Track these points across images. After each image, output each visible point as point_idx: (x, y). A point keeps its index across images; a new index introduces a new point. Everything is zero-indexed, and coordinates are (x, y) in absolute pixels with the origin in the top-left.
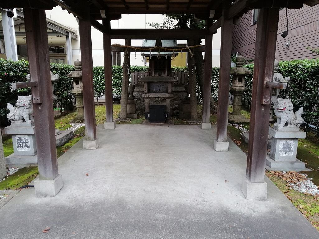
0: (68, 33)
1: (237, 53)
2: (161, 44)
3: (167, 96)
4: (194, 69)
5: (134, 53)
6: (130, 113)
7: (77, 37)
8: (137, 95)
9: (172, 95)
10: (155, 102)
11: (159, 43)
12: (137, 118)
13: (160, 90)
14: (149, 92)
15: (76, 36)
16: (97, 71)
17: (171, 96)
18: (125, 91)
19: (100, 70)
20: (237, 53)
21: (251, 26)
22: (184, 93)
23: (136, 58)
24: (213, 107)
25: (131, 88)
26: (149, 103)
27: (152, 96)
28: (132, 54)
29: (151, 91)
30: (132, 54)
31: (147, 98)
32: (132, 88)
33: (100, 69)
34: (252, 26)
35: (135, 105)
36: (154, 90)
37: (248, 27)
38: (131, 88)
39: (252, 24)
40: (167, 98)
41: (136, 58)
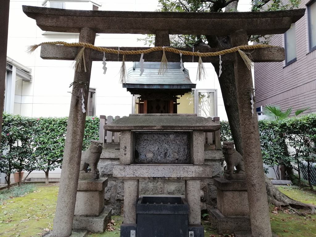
0: (11, 67)
1: (261, 107)
2: (167, 42)
3: (190, 171)
4: (253, 95)
5: (100, 63)
6: (87, 216)
7: (30, 79)
8: (109, 167)
9: (208, 169)
10: (149, 183)
11: (162, 40)
12: (102, 231)
13: (166, 153)
14: (136, 159)
15: (30, 76)
16: (48, 124)
17: (204, 171)
18: (71, 159)
19: (53, 123)
20: (261, 107)
21: (284, 68)
22: (214, 163)
23: (105, 73)
24: (272, 193)
25: (92, 150)
26: (134, 194)
27: (144, 171)
28: (96, 66)
29: (142, 157)
30: (96, 66)
31: (130, 179)
32: (94, 151)
33: (54, 121)
34: (285, 68)
35: (102, 192)
36: (150, 156)
37: (278, 70)
38: (92, 150)
39: (308, 51)
40: (193, 179)
41: (105, 73)
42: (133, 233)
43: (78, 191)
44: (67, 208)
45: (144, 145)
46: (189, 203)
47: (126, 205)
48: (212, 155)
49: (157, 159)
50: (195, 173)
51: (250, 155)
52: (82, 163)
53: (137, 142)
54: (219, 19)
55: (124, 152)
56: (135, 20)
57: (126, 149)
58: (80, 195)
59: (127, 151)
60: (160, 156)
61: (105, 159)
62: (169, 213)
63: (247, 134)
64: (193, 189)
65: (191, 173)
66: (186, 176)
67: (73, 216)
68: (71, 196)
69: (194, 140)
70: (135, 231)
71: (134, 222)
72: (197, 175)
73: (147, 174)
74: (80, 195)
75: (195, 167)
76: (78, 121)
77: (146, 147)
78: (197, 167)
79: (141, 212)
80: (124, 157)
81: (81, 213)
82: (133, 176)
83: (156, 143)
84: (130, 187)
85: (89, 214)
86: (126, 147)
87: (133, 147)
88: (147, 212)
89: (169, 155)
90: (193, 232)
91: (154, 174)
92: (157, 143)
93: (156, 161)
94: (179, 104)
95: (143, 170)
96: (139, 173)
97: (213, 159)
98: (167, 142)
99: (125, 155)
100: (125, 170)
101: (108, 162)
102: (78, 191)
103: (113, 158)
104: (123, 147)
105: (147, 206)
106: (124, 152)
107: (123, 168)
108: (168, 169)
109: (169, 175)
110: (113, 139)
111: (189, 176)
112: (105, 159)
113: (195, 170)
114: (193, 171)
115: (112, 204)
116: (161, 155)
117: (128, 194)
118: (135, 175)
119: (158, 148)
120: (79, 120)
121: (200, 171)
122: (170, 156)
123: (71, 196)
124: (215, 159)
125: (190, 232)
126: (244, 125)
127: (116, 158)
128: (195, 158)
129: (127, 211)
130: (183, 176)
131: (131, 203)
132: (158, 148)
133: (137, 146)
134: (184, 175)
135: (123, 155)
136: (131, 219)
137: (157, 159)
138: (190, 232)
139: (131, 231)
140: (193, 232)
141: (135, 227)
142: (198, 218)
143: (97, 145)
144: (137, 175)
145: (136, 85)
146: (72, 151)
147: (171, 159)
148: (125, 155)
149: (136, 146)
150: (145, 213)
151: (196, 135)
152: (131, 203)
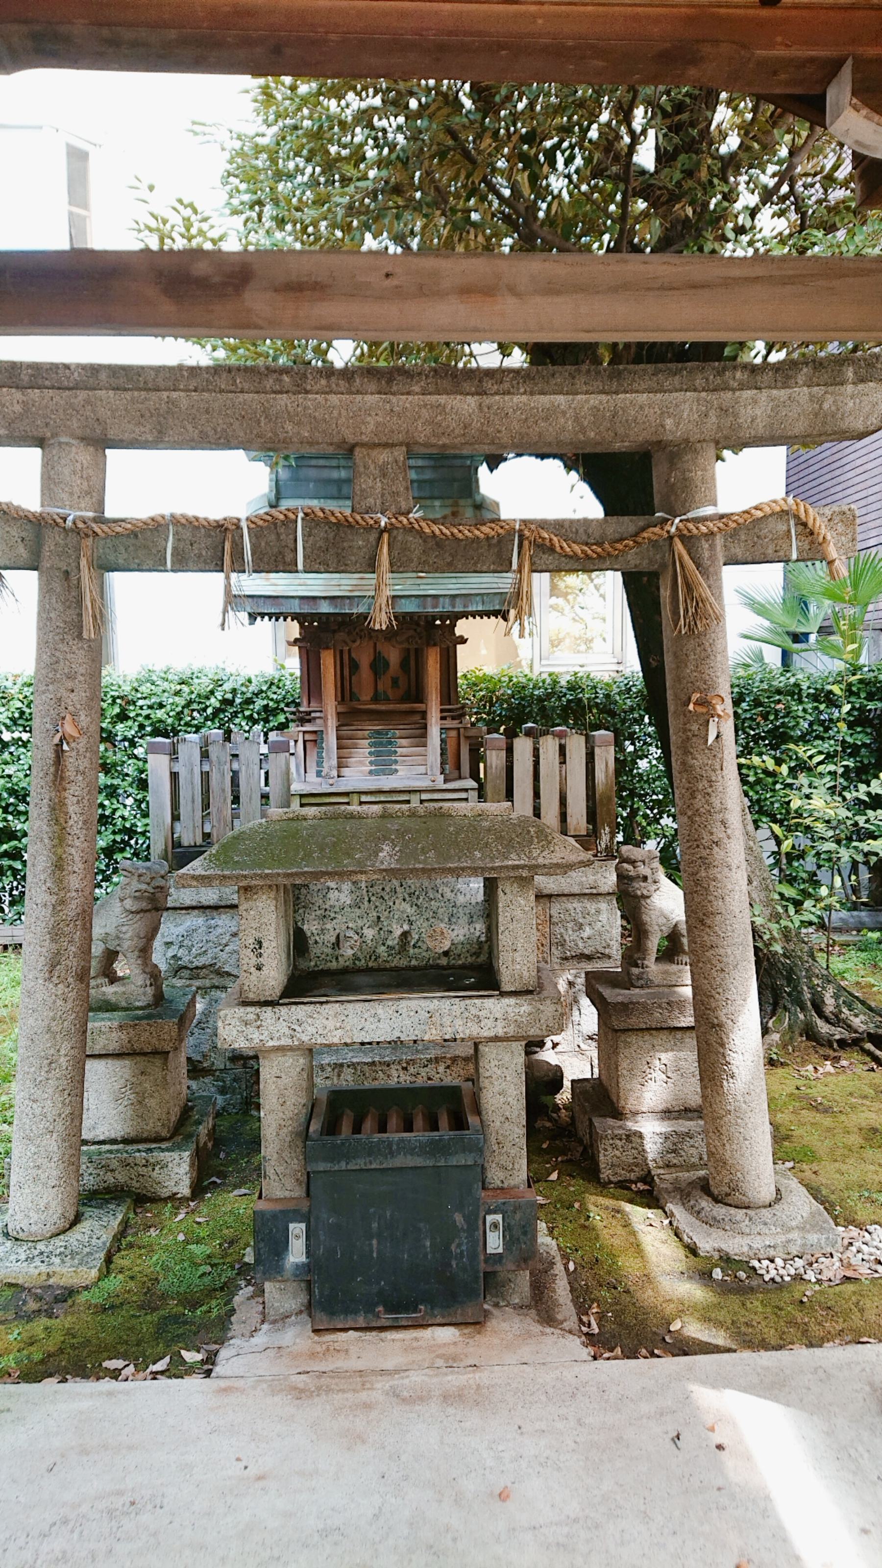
6: (126, 1141)
12: (184, 1190)
25: (129, 904)
42: (297, 1231)
43: (88, 1056)
44: (55, 1135)
45: (327, 907)
46: (485, 1118)
47: (268, 1136)
48: (584, 879)
49: (373, 958)
50: (503, 1024)
51: (708, 922)
52: (97, 949)
53: (298, 898)
54: (604, 397)
55: (254, 961)
56: (268, 401)
57: (260, 948)
58: (93, 1067)
59: (265, 955)
60: (384, 944)
61: (182, 909)
62: (419, 1161)
63: (698, 846)
64: (499, 1072)
65: (490, 1023)
66: (475, 1034)
67: (75, 1141)
68: (66, 1092)
69: (500, 910)
70: (303, 1226)
71: (299, 1192)
72: (511, 1030)
73: (339, 1033)
74: (93, 1067)
75: (506, 1001)
76: (71, 822)
77: (333, 915)
78: (512, 1001)
79: (322, 1166)
80: (253, 978)
81: (102, 1132)
82: (289, 1042)
83: (369, 901)
84: (283, 1075)
85: (133, 1134)
86: (260, 943)
87: (286, 916)
88: (343, 1165)
89: (418, 941)
90: (499, 1218)
91: (363, 1033)
92: (373, 899)
93: (370, 964)
94: (463, 641)
95: (324, 1021)
96: (311, 1030)
97: (587, 891)
98: (410, 895)
99: (259, 968)
100: (259, 1023)
101: (196, 921)
102: (88, 1056)
103: (211, 903)
104: (251, 941)
105: (343, 1144)
106: (254, 961)
107: (252, 1017)
108: (412, 1014)
109: (416, 1032)
110: (207, 829)
111: (485, 1034)
112: (182, 909)
113: (503, 1011)
114: (498, 1015)
115: (217, 1073)
116: (389, 943)
117: (275, 1100)
118: (299, 1039)
119: (379, 918)
120: (73, 816)
121: (522, 1016)
122: (420, 944)
123: (66, 1092)
124: (595, 891)
125: (490, 1218)
126: (690, 813)
127: (222, 904)
128: (503, 969)
129: (275, 1156)
130: (462, 1036)
131: (285, 1130)
132: (379, 918)
133: (301, 911)
134: (468, 1032)
135: (253, 970)
136: (290, 1183)
137: (373, 958)
138: (490, 1218)
139: (291, 1226)
140: (499, 1218)
141: (305, 1209)
142: (517, 1166)
143: (148, 884)
144: (305, 1038)
145: (283, 601)
146: (55, 934)
147: (424, 954)
148: (259, 968)
149: (295, 912)
150: (336, 1168)
151: (507, 891)
152: (285, 1130)
